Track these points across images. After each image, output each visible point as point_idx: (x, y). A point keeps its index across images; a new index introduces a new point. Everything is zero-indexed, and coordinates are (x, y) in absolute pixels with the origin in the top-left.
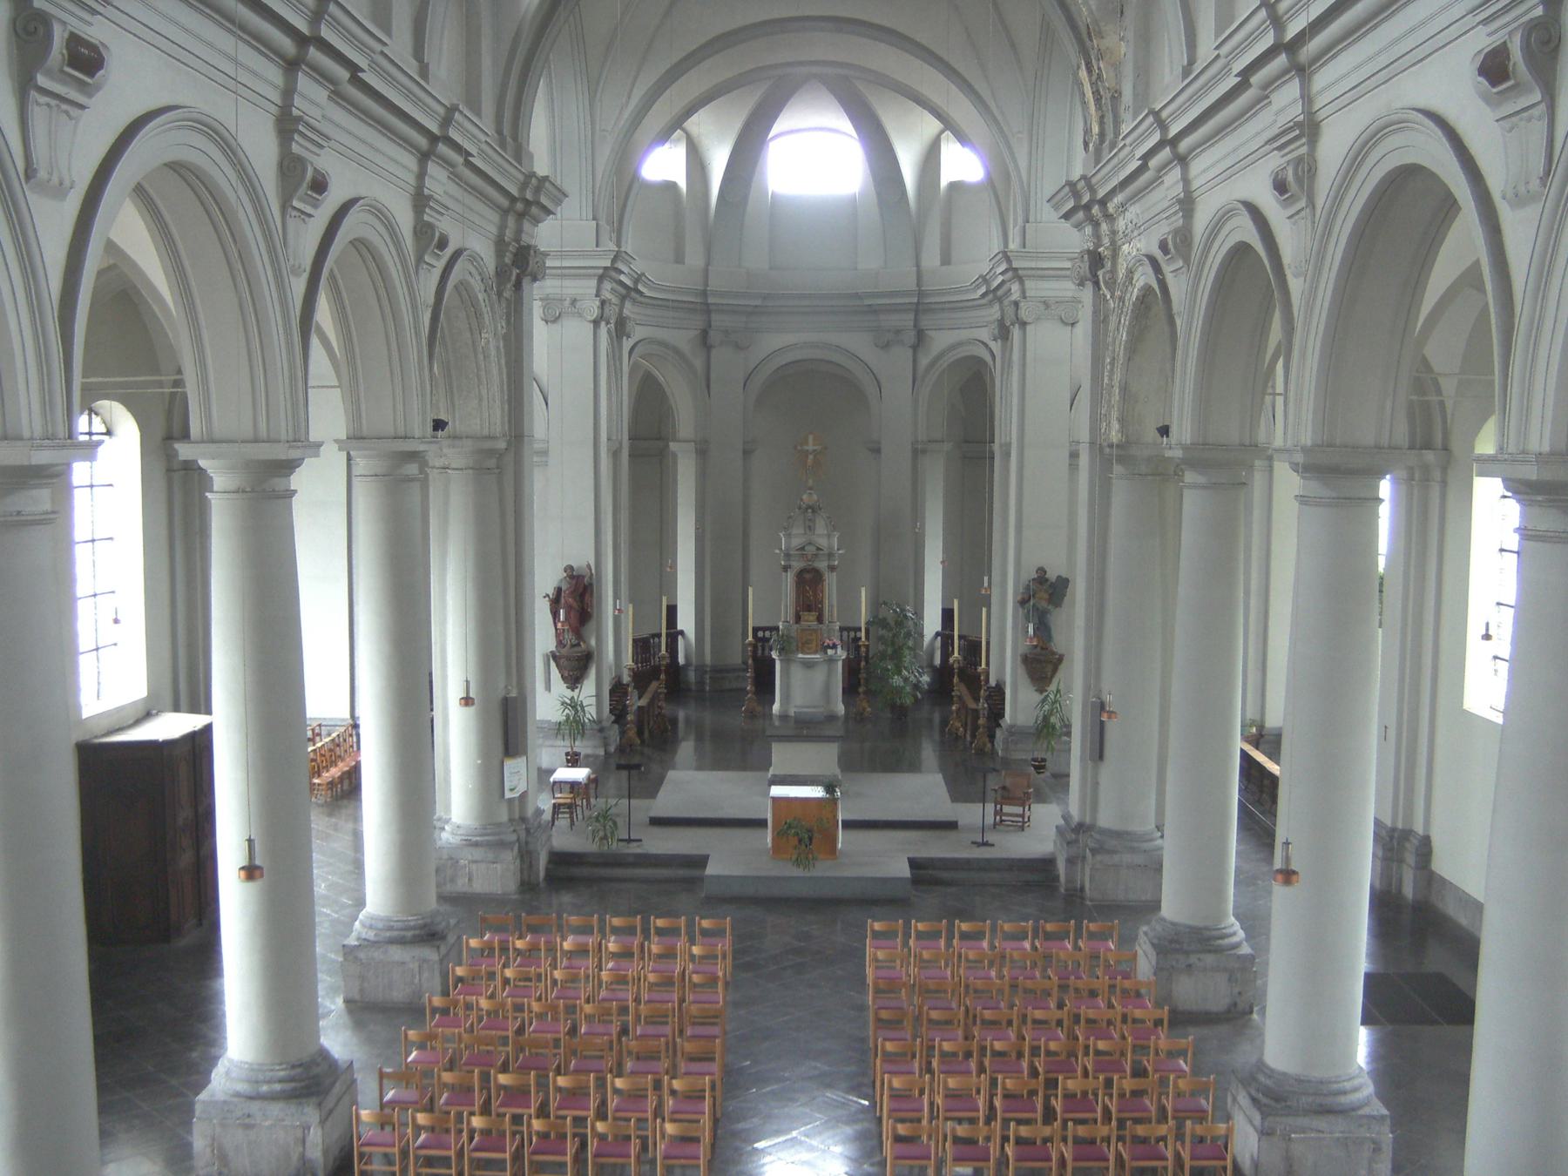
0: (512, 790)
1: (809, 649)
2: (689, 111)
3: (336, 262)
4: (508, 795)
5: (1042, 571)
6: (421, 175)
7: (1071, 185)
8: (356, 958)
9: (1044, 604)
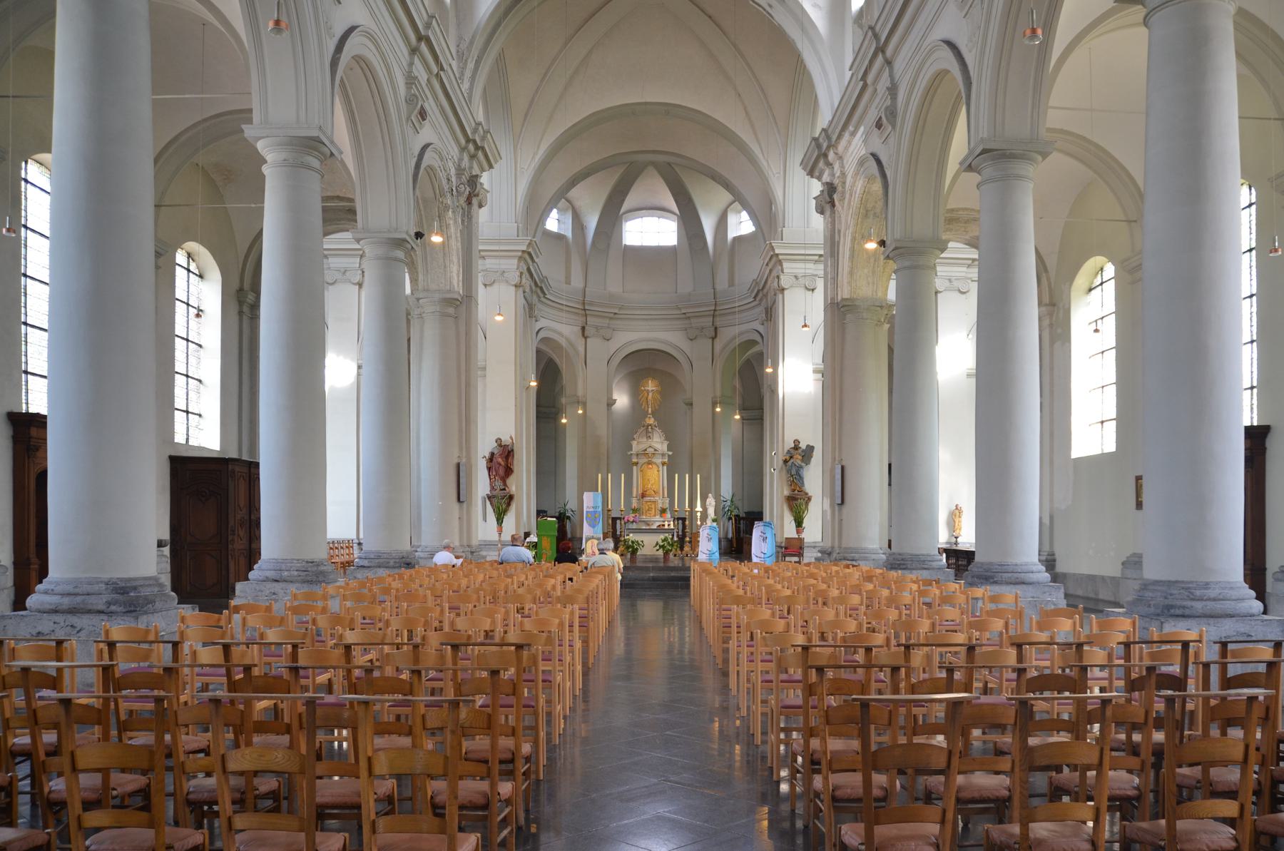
2: (573, 182)
3: (344, 72)
5: (797, 442)
6: (411, 64)
7: (815, 140)
8: (355, 578)
9: (799, 462)
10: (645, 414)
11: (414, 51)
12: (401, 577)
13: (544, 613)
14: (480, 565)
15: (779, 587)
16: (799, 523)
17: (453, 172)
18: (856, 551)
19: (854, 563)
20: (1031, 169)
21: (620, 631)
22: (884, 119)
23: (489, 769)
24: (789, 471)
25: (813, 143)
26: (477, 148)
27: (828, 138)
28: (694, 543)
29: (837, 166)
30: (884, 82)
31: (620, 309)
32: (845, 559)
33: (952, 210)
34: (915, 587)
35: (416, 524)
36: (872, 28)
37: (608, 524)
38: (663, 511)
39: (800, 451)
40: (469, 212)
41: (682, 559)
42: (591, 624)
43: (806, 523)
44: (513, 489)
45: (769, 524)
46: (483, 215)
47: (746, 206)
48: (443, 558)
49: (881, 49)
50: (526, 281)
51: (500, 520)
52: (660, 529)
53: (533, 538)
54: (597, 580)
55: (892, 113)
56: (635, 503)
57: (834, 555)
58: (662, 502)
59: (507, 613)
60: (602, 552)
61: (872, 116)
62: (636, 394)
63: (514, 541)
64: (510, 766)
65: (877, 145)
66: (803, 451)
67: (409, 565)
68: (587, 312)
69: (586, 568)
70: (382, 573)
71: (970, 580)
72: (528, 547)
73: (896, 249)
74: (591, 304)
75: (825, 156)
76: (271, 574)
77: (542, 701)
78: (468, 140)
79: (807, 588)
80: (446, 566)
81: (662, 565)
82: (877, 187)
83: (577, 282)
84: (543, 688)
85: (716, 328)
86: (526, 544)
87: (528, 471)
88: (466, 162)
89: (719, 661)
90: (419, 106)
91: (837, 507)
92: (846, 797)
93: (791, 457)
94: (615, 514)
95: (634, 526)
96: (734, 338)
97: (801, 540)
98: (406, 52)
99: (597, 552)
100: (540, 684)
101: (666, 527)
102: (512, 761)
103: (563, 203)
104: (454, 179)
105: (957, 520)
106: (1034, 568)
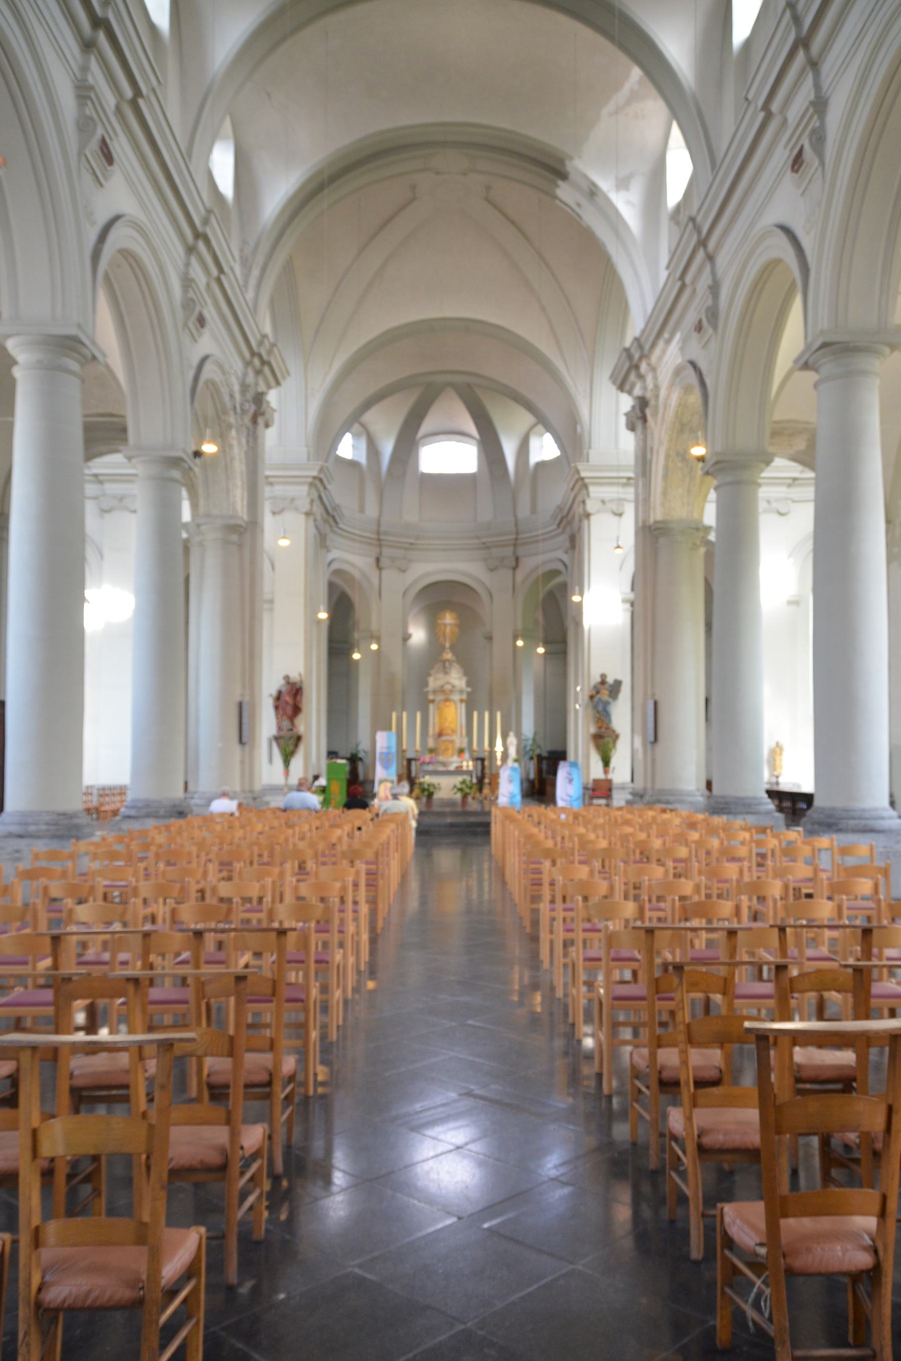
2: (367, 405)
5: (603, 676)
6: (188, 265)
7: (627, 350)
10: (443, 648)
11: (191, 250)
12: (168, 828)
13: (325, 873)
14: (260, 813)
15: (592, 836)
16: (606, 762)
17: (236, 388)
18: (672, 792)
19: (670, 806)
21: (414, 885)
22: (705, 322)
23: (229, 1113)
24: (595, 707)
26: (263, 362)
27: (641, 347)
28: (494, 785)
29: (649, 379)
30: (705, 280)
31: (417, 538)
32: (659, 801)
33: (776, 422)
34: (747, 835)
35: (190, 767)
36: (692, 219)
37: (403, 765)
38: (461, 751)
39: (607, 686)
40: (255, 432)
41: (481, 802)
42: (381, 883)
43: (614, 762)
44: (301, 728)
45: (575, 765)
46: (270, 437)
47: (549, 428)
48: (222, 806)
49: (703, 243)
50: (318, 509)
51: (287, 762)
52: (459, 771)
53: (322, 782)
54: (388, 831)
55: (713, 314)
56: (431, 743)
57: (647, 798)
58: (460, 741)
59: (282, 875)
60: (395, 797)
61: (691, 318)
62: (433, 628)
63: (300, 787)
64: (267, 1090)
65: (695, 351)
66: (611, 686)
67: (181, 814)
68: (383, 543)
69: (377, 815)
70: (150, 823)
71: (809, 827)
72: (315, 792)
73: (717, 463)
74: (386, 533)
75: (637, 367)
76: (15, 829)
77: (314, 992)
78: (253, 354)
79: (625, 838)
80: (222, 815)
81: (459, 809)
82: (695, 398)
83: (372, 511)
84: (316, 973)
85: (517, 559)
86: (314, 789)
87: (318, 710)
88: (251, 378)
89: (527, 923)
91: (649, 746)
92: (717, 1146)
94: (410, 755)
95: (430, 768)
96: (537, 568)
97: (609, 782)
98: (181, 250)
99: (390, 797)
100: (313, 966)
101: (465, 768)
102: (269, 1084)
103: (356, 426)
104: (237, 396)
105: (778, 758)
106: (885, 814)
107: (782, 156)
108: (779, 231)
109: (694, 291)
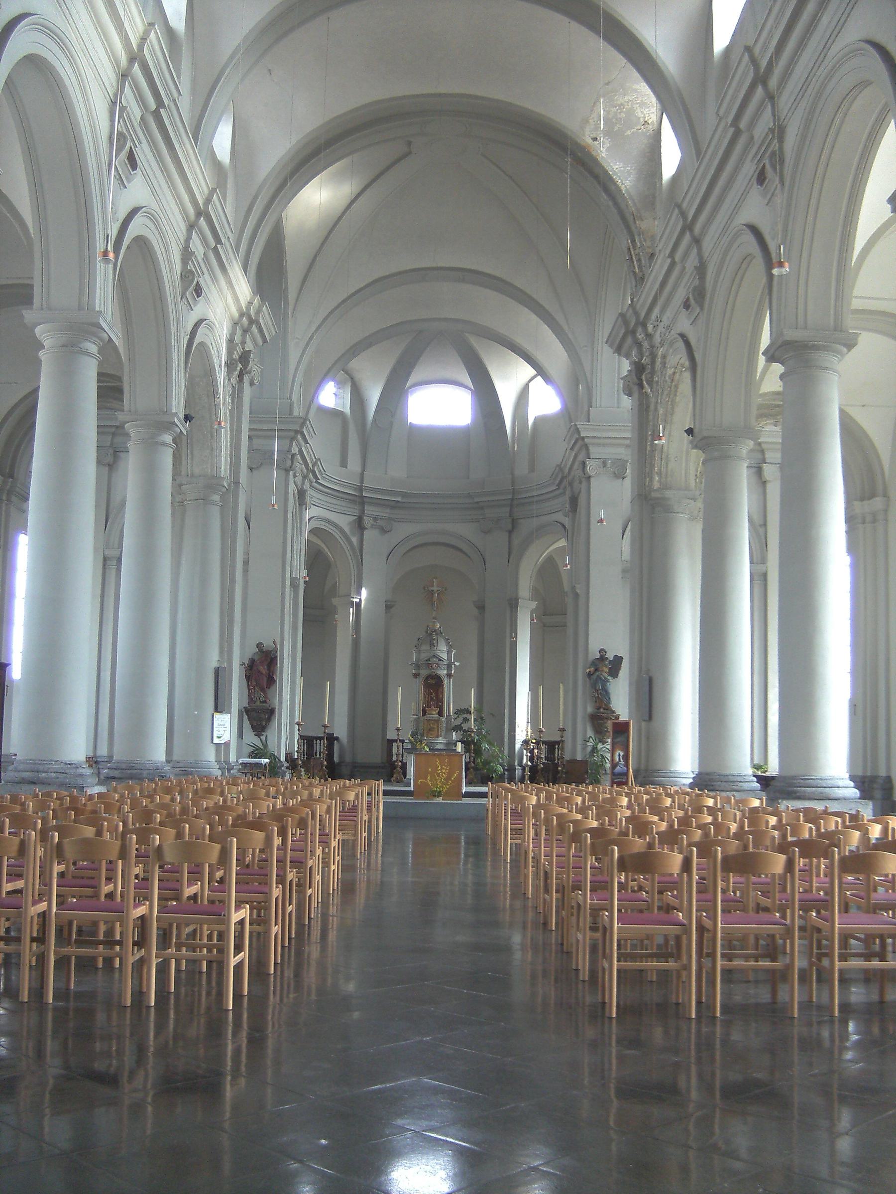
0: (219, 737)
1: (431, 734)
2: (355, 350)
4: (216, 741)
6: (188, 239)
20: (835, 360)
25: (620, 319)
30: (692, 261)
49: (688, 227)
61: (681, 295)
68: (365, 500)
75: (633, 332)
83: (354, 464)
90: (195, 283)
93: (596, 670)
94: (391, 735)
98: (183, 227)
106: (841, 783)
107: (749, 169)
108: (748, 232)
109: (684, 268)
